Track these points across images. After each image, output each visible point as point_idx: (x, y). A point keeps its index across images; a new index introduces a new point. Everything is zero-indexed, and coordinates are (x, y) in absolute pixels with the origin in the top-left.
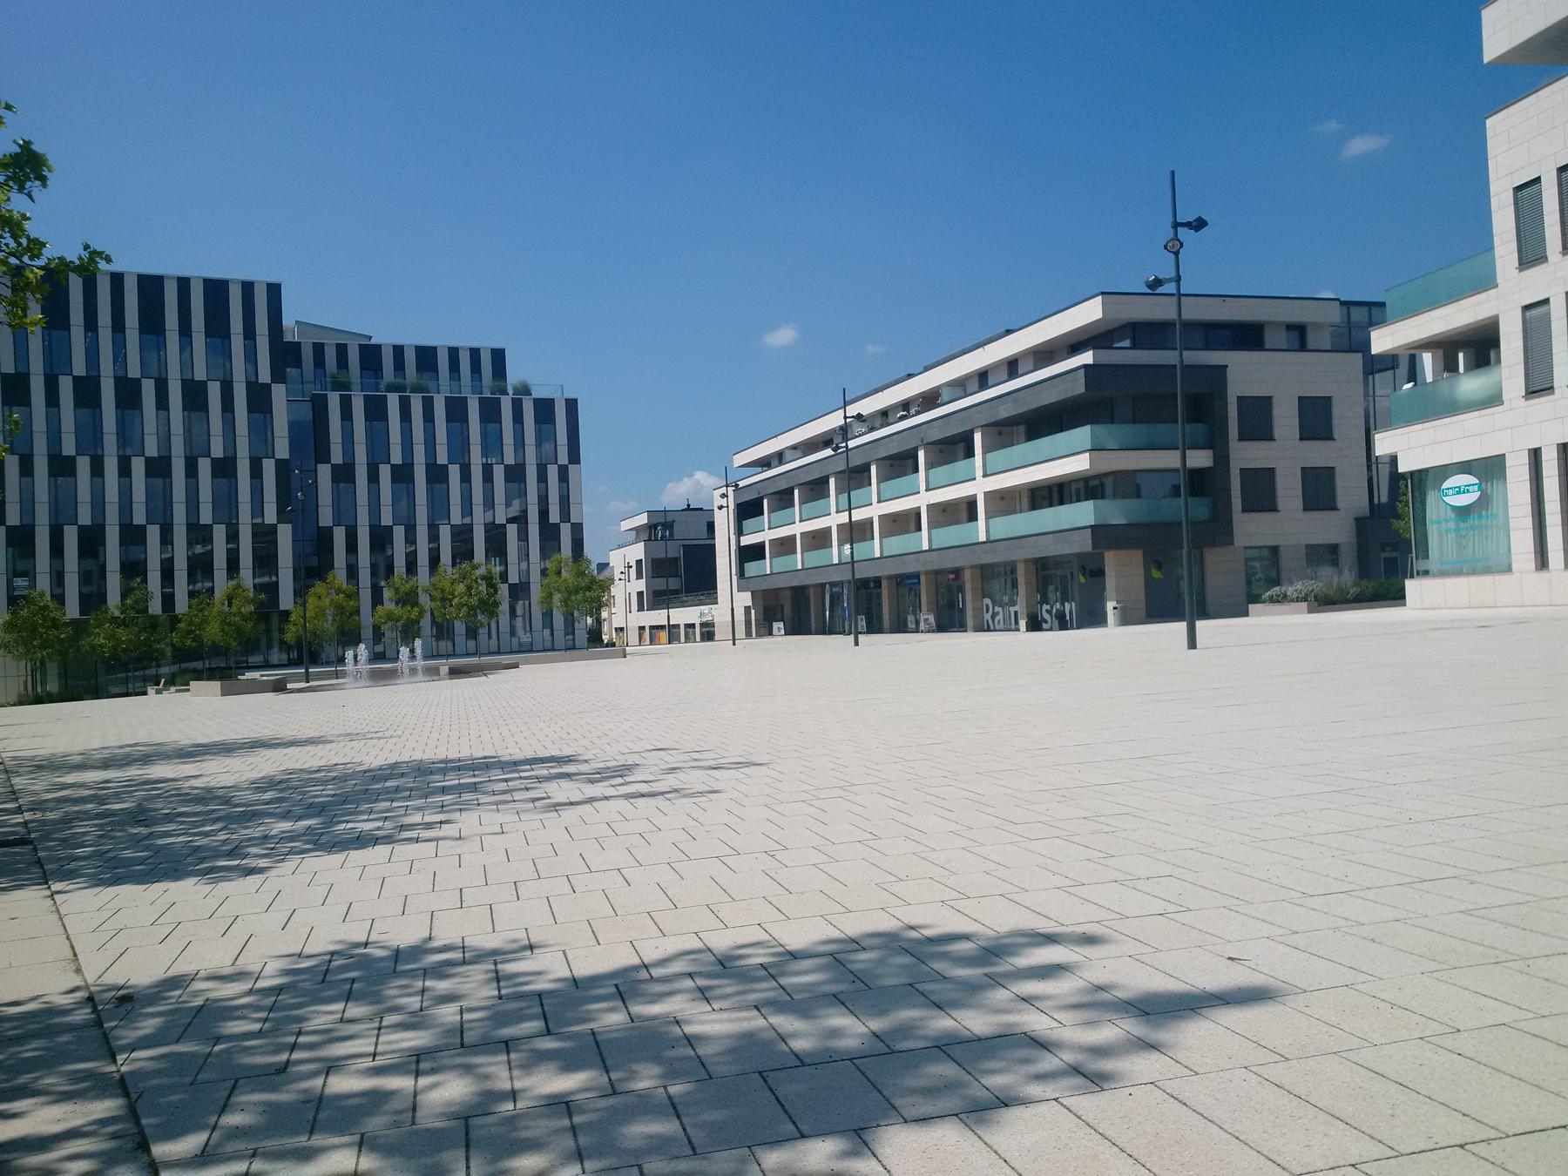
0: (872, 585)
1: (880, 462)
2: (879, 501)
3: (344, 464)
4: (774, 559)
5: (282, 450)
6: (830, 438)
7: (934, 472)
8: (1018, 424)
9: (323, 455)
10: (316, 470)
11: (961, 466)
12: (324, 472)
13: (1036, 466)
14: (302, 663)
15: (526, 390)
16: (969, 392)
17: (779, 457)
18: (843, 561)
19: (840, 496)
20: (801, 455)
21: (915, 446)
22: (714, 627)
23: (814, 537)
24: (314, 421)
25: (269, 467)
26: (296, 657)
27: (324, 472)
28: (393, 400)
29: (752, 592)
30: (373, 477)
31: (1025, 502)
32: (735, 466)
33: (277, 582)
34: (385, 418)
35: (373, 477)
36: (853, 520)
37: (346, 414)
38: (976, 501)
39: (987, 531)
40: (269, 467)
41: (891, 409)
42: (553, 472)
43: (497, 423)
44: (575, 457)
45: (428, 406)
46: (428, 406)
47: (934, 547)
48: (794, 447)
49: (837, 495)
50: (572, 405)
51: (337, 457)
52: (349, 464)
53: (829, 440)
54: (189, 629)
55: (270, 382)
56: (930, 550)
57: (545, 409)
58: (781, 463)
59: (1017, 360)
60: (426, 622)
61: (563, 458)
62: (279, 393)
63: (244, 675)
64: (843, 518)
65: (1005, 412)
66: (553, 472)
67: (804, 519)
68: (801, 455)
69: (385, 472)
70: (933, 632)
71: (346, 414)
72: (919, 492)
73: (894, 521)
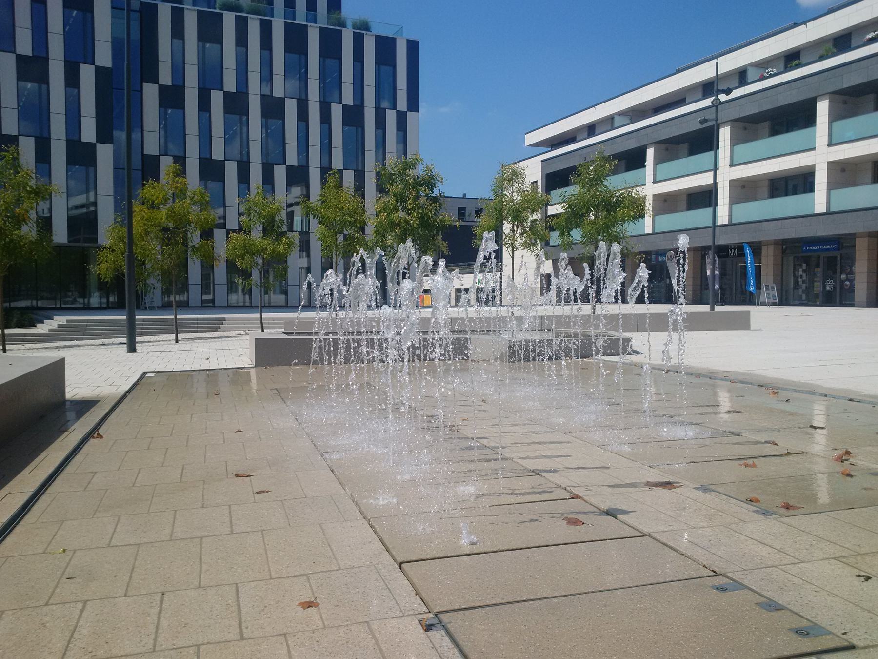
0: (732, 253)
1: (837, 96)
2: (655, 182)
3: (173, 85)
4: (734, 206)
5: (104, 56)
6: (684, 97)
7: (838, 125)
8: (683, 142)
9: (150, 74)
10: (141, 91)
12: (151, 92)
13: (806, 153)
14: (124, 306)
15: (366, 26)
16: (616, 126)
17: (609, 122)
18: (656, 231)
20: (629, 121)
23: (843, 170)
24: (141, 39)
25: (87, 74)
26: (116, 301)
27: (151, 92)
28: (229, 20)
29: (553, 260)
30: (204, 105)
31: (765, 191)
32: (526, 145)
33: (96, 211)
34: (219, 41)
35: (204, 105)
37: (178, 31)
38: (815, 172)
39: (730, 216)
40: (87, 74)
41: (598, 123)
42: (391, 118)
43: (279, 119)
44: (413, 104)
45: (266, 29)
46: (266, 29)
48: (622, 114)
49: (831, 122)
50: (413, 47)
51: (165, 77)
52: (177, 86)
55: (99, 146)
56: (653, 234)
57: (386, 47)
61: (402, 103)
62: (105, 154)
63: (68, 321)
65: (752, 109)
66: (391, 118)
67: (833, 142)
69: (217, 98)
70: (774, 304)
71: (178, 31)
72: (645, 185)
73: (744, 187)
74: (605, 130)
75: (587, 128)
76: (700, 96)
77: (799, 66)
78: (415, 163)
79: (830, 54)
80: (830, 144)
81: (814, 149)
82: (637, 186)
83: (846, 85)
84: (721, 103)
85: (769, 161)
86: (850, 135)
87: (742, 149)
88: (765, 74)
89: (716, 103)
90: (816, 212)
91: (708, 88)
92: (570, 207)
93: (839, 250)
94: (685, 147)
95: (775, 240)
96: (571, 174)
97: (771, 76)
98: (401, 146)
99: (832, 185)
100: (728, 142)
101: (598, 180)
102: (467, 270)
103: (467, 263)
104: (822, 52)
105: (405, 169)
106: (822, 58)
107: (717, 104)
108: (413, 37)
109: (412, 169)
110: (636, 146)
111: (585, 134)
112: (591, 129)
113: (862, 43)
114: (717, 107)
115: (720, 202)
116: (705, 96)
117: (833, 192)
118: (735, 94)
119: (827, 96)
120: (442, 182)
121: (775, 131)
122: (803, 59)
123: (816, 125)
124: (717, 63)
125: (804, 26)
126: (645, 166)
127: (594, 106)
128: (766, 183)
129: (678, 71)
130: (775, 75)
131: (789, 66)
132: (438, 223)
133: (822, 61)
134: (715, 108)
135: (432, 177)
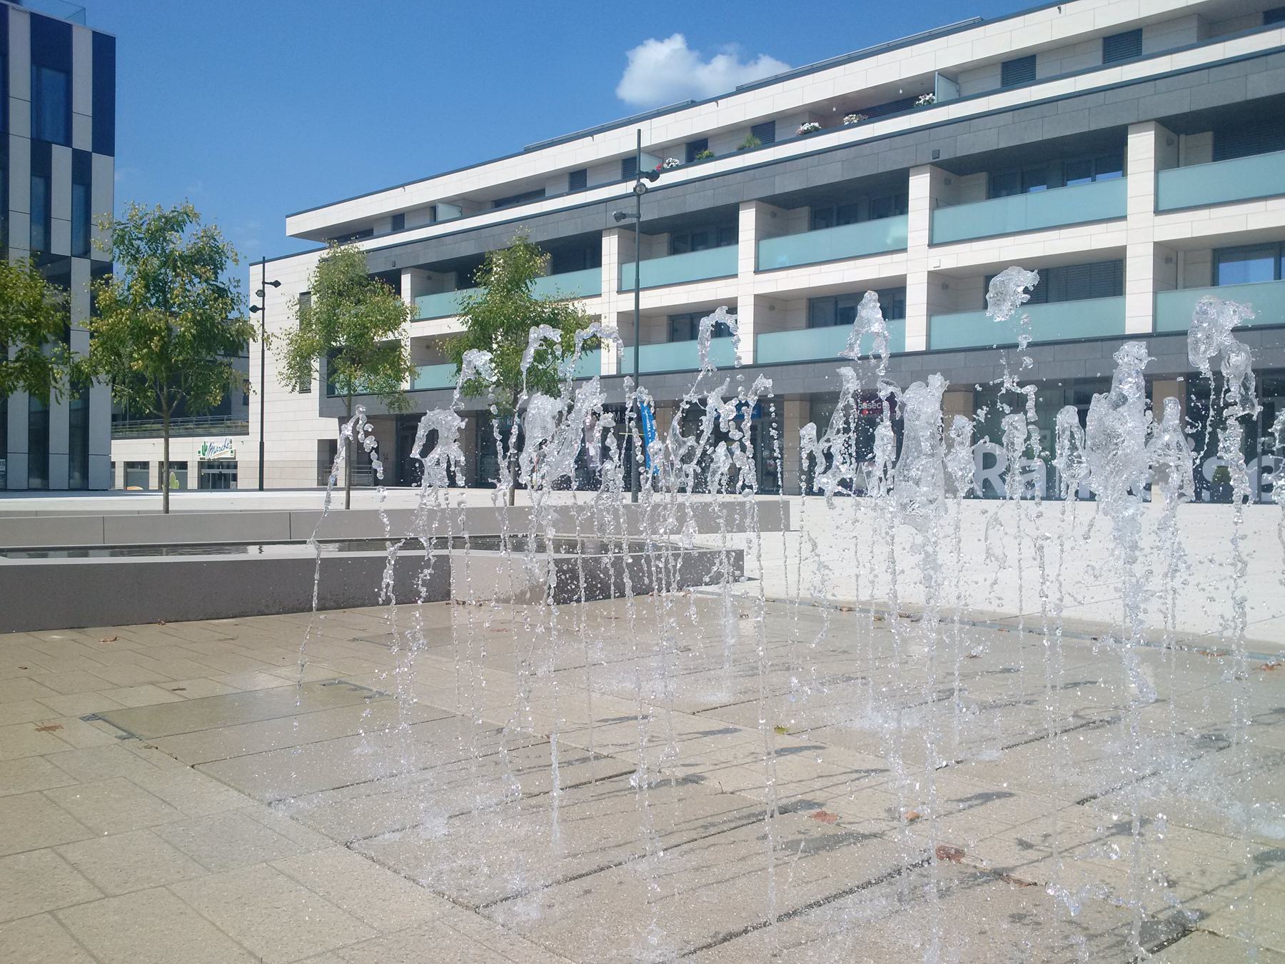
11: (890, 227)
16: (440, 218)
17: (430, 212)
19: (625, 267)
21: (732, 200)
22: (235, 467)
31: (803, 316)
32: (288, 234)
36: (640, 308)
38: (905, 288)
39: (755, 351)
42: (61, 159)
44: (104, 140)
47: (934, 347)
50: (104, 47)
53: (367, 231)
54: (1234, 663)
58: (434, 221)
59: (773, 123)
60: (1132, 359)
61: (83, 137)
64: (627, 303)
68: (458, 215)
74: (417, 225)
75: (1100, 42)
76: (566, 188)
77: (711, 158)
78: (184, 222)
79: (753, 146)
80: (757, 271)
81: (736, 276)
82: (575, 299)
83: (778, 190)
84: (648, 191)
85: (790, 272)
86: (783, 260)
87: (949, 215)
88: (665, 166)
89: (641, 190)
90: (907, 350)
91: (628, 165)
92: (475, 321)
93: (760, 417)
94: (981, 179)
95: (802, 394)
96: (476, 267)
97: (672, 169)
98: (39, 230)
99: (935, 308)
100: (615, 258)
101: (518, 280)
102: (223, 429)
103: (180, 419)
104: (743, 142)
105: (163, 230)
106: (742, 150)
107: (638, 193)
108: (104, 29)
109: (178, 231)
110: (476, 252)
111: (389, 228)
112: (398, 221)
113: (794, 136)
114: (639, 196)
115: (1130, 286)
116: (626, 178)
117: (761, 337)
118: (665, 179)
119: (754, 203)
120: (236, 260)
121: (1223, 151)
122: (1147, 46)
123: (737, 242)
124: (639, 131)
125: (590, 138)
126: (600, 265)
127: (403, 186)
128: (665, 320)
129: (527, 151)
130: (678, 168)
131: (698, 157)
132: (232, 336)
133: (806, 139)
134: (635, 198)
135: (219, 251)
